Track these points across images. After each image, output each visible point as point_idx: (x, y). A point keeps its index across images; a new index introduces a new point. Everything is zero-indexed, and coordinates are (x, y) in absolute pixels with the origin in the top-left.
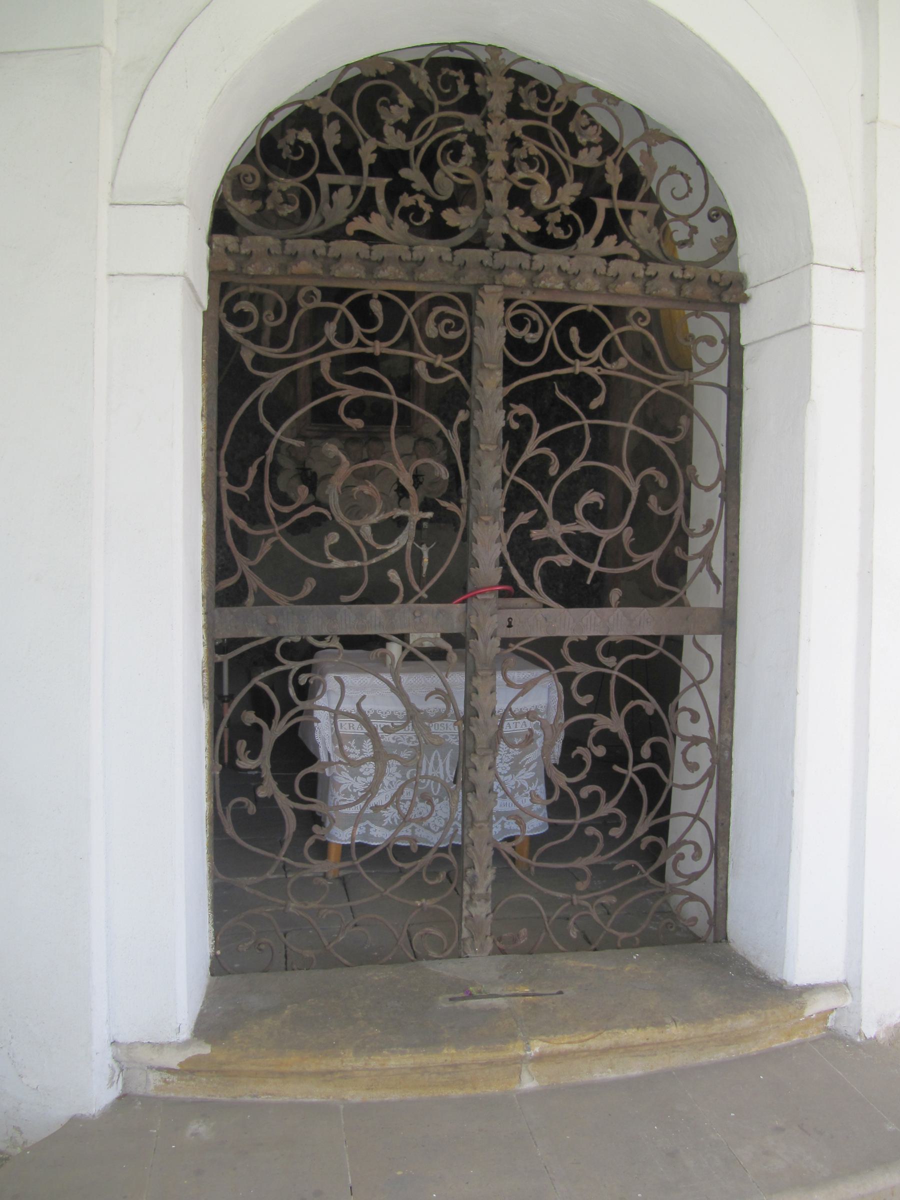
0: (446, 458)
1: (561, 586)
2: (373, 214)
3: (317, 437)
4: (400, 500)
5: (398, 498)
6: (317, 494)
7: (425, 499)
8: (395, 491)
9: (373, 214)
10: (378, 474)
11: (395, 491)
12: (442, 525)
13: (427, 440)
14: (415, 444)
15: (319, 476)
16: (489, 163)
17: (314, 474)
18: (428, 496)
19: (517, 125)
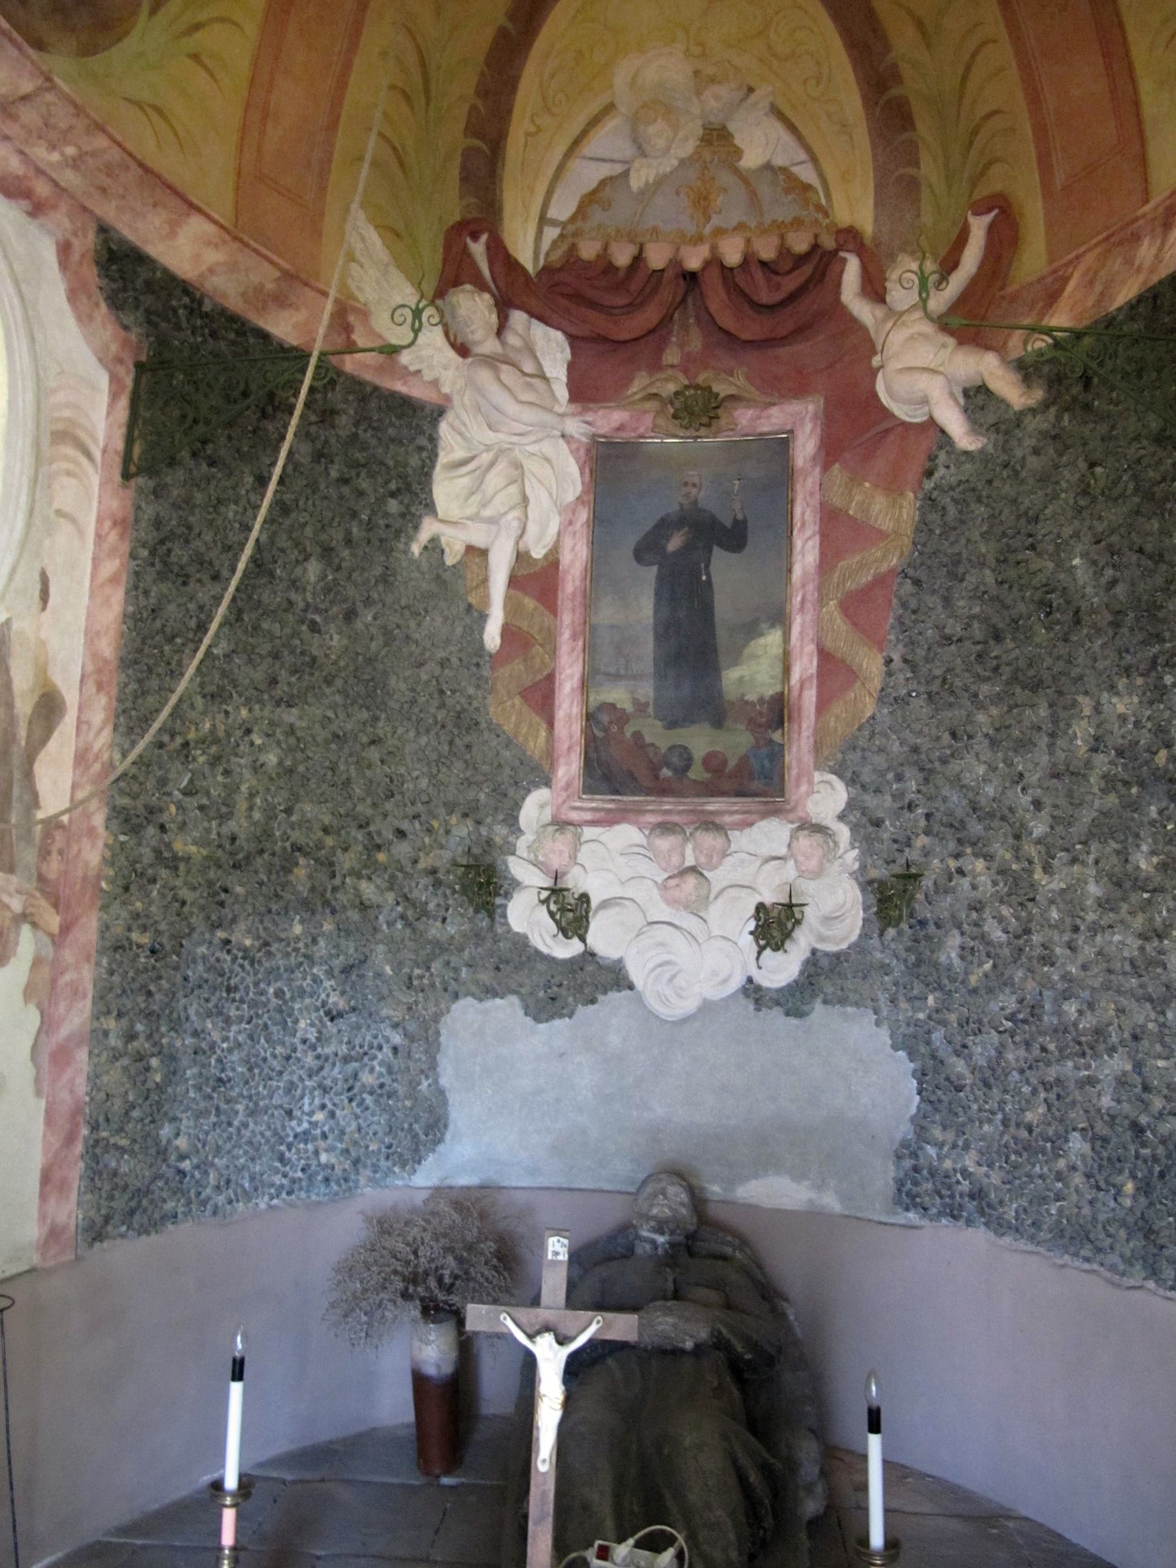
0: (856, 866)
1: (1129, 1187)
2: (538, 553)
3: (593, 823)
4: (759, 953)
5: (755, 948)
6: (590, 938)
7: (814, 952)
8: (751, 933)
9: (538, 553)
10: (716, 897)
11: (751, 933)
12: (850, 1009)
13: (819, 829)
14: (793, 836)
15: (594, 903)
16: (600, 1497)
17: (584, 898)
18: (820, 946)
19: (1022, 663)
